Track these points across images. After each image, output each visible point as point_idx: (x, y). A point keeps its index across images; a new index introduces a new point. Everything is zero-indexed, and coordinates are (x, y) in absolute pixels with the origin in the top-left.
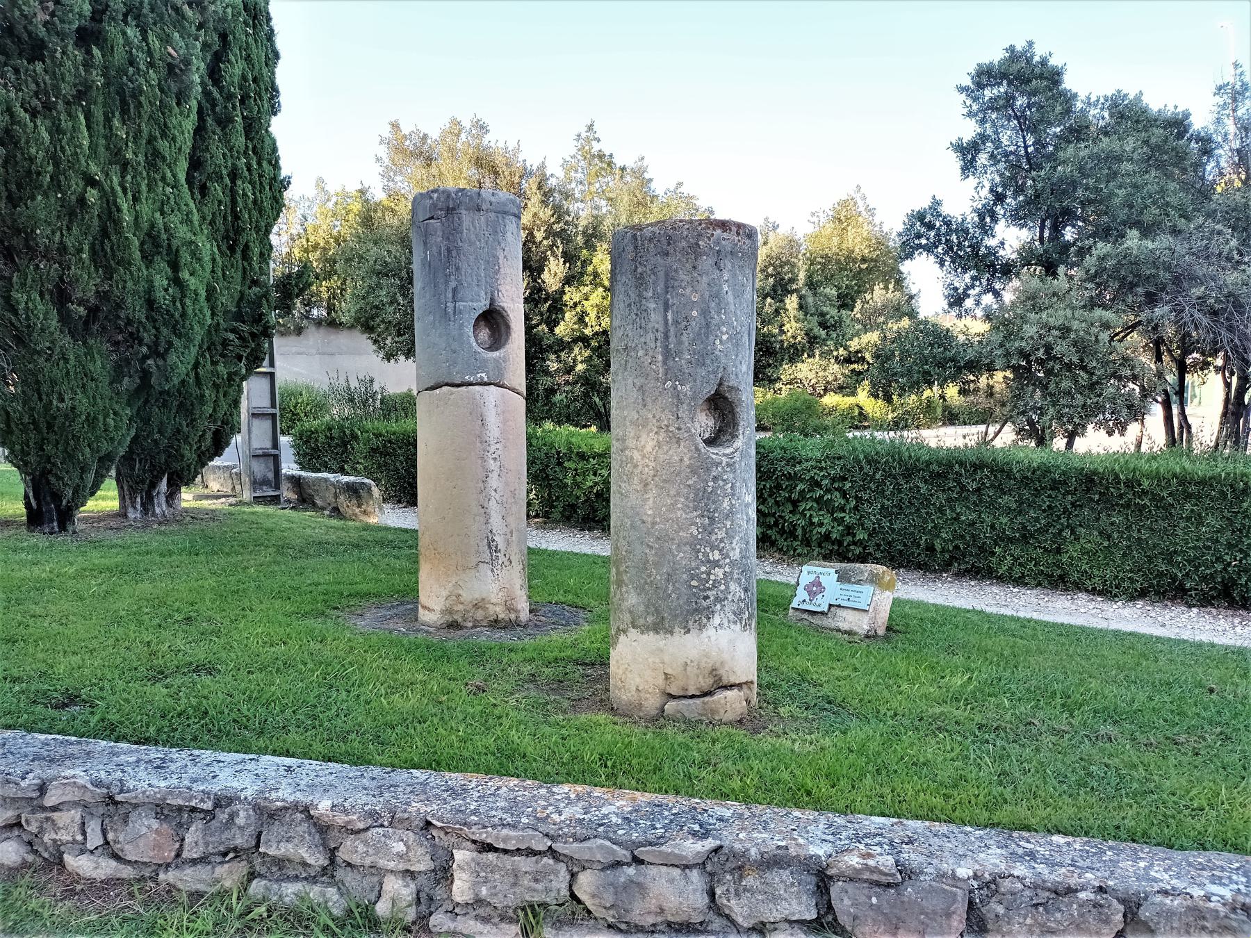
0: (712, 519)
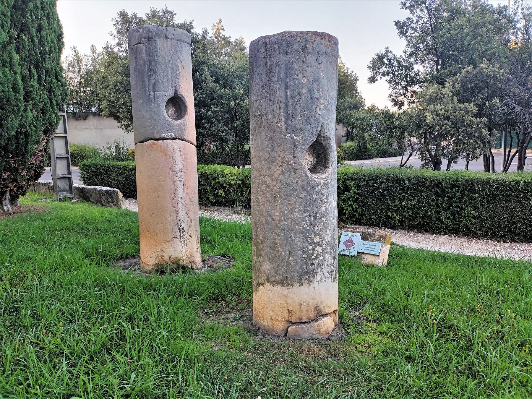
0: (315, 218)
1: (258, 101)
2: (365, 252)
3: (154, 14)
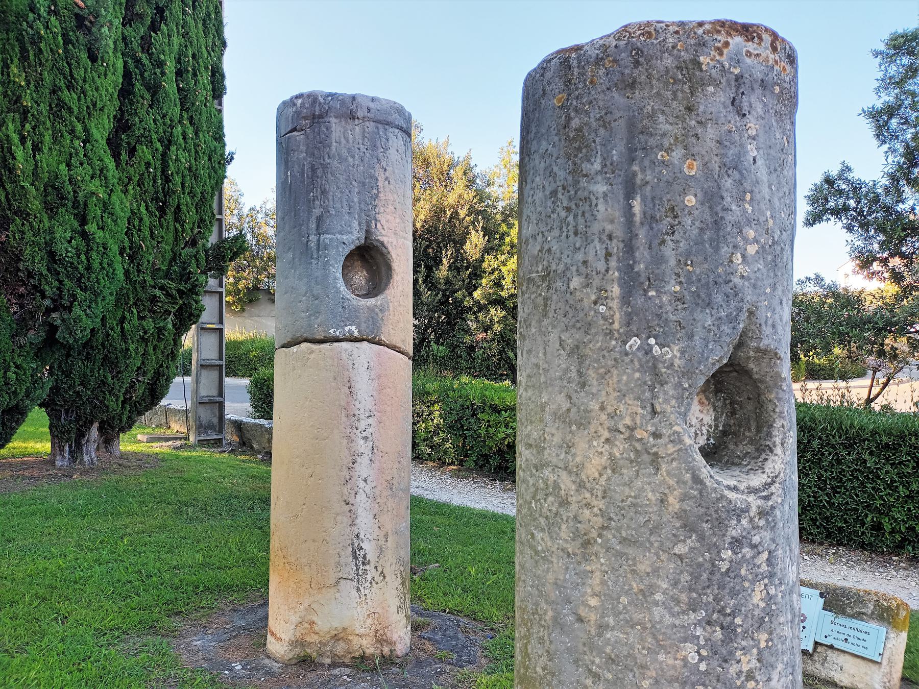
0: (729, 631)
1: (539, 238)
2: (837, 644)
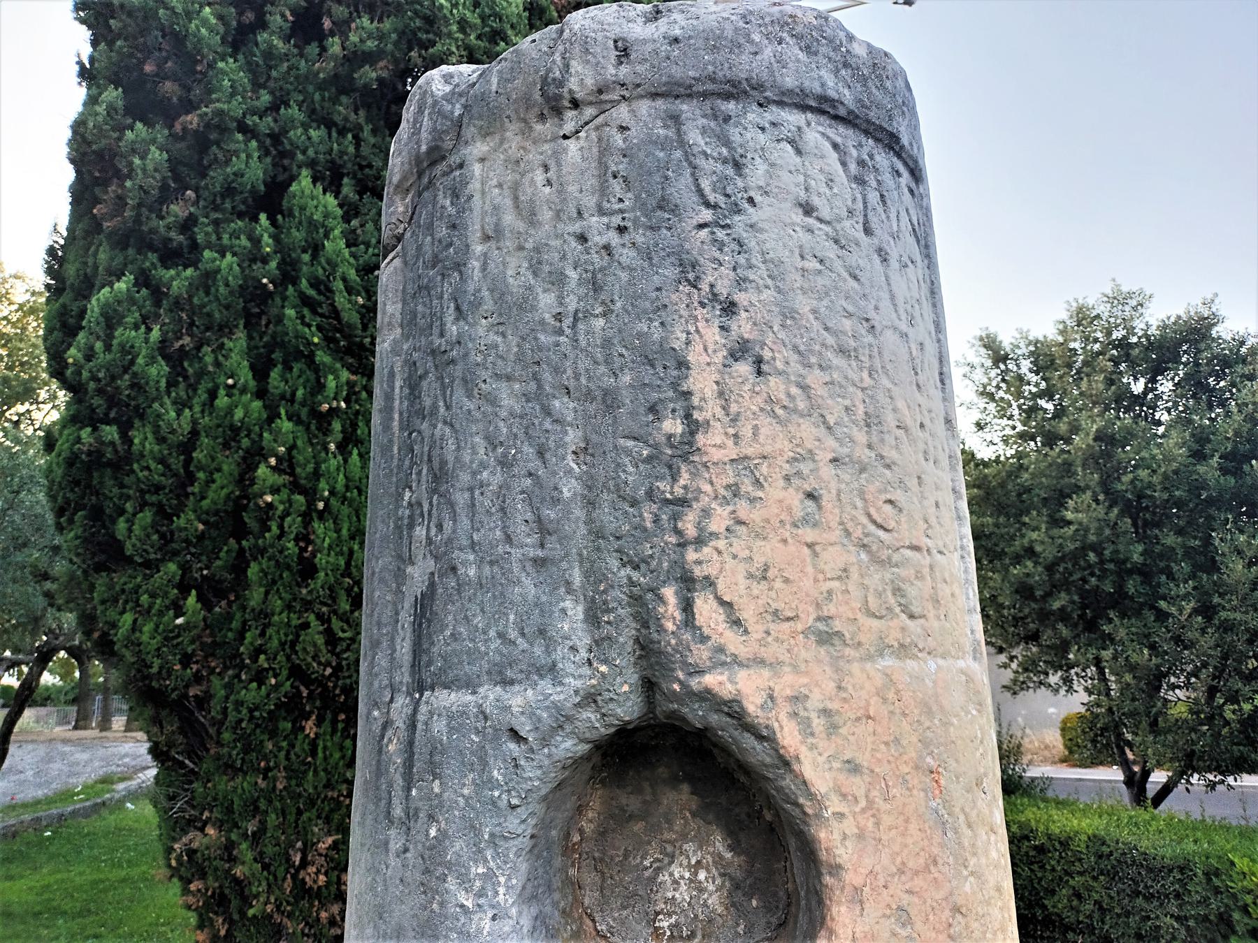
3: (1083, 318)
